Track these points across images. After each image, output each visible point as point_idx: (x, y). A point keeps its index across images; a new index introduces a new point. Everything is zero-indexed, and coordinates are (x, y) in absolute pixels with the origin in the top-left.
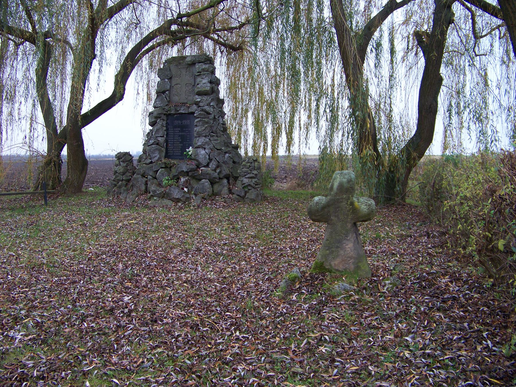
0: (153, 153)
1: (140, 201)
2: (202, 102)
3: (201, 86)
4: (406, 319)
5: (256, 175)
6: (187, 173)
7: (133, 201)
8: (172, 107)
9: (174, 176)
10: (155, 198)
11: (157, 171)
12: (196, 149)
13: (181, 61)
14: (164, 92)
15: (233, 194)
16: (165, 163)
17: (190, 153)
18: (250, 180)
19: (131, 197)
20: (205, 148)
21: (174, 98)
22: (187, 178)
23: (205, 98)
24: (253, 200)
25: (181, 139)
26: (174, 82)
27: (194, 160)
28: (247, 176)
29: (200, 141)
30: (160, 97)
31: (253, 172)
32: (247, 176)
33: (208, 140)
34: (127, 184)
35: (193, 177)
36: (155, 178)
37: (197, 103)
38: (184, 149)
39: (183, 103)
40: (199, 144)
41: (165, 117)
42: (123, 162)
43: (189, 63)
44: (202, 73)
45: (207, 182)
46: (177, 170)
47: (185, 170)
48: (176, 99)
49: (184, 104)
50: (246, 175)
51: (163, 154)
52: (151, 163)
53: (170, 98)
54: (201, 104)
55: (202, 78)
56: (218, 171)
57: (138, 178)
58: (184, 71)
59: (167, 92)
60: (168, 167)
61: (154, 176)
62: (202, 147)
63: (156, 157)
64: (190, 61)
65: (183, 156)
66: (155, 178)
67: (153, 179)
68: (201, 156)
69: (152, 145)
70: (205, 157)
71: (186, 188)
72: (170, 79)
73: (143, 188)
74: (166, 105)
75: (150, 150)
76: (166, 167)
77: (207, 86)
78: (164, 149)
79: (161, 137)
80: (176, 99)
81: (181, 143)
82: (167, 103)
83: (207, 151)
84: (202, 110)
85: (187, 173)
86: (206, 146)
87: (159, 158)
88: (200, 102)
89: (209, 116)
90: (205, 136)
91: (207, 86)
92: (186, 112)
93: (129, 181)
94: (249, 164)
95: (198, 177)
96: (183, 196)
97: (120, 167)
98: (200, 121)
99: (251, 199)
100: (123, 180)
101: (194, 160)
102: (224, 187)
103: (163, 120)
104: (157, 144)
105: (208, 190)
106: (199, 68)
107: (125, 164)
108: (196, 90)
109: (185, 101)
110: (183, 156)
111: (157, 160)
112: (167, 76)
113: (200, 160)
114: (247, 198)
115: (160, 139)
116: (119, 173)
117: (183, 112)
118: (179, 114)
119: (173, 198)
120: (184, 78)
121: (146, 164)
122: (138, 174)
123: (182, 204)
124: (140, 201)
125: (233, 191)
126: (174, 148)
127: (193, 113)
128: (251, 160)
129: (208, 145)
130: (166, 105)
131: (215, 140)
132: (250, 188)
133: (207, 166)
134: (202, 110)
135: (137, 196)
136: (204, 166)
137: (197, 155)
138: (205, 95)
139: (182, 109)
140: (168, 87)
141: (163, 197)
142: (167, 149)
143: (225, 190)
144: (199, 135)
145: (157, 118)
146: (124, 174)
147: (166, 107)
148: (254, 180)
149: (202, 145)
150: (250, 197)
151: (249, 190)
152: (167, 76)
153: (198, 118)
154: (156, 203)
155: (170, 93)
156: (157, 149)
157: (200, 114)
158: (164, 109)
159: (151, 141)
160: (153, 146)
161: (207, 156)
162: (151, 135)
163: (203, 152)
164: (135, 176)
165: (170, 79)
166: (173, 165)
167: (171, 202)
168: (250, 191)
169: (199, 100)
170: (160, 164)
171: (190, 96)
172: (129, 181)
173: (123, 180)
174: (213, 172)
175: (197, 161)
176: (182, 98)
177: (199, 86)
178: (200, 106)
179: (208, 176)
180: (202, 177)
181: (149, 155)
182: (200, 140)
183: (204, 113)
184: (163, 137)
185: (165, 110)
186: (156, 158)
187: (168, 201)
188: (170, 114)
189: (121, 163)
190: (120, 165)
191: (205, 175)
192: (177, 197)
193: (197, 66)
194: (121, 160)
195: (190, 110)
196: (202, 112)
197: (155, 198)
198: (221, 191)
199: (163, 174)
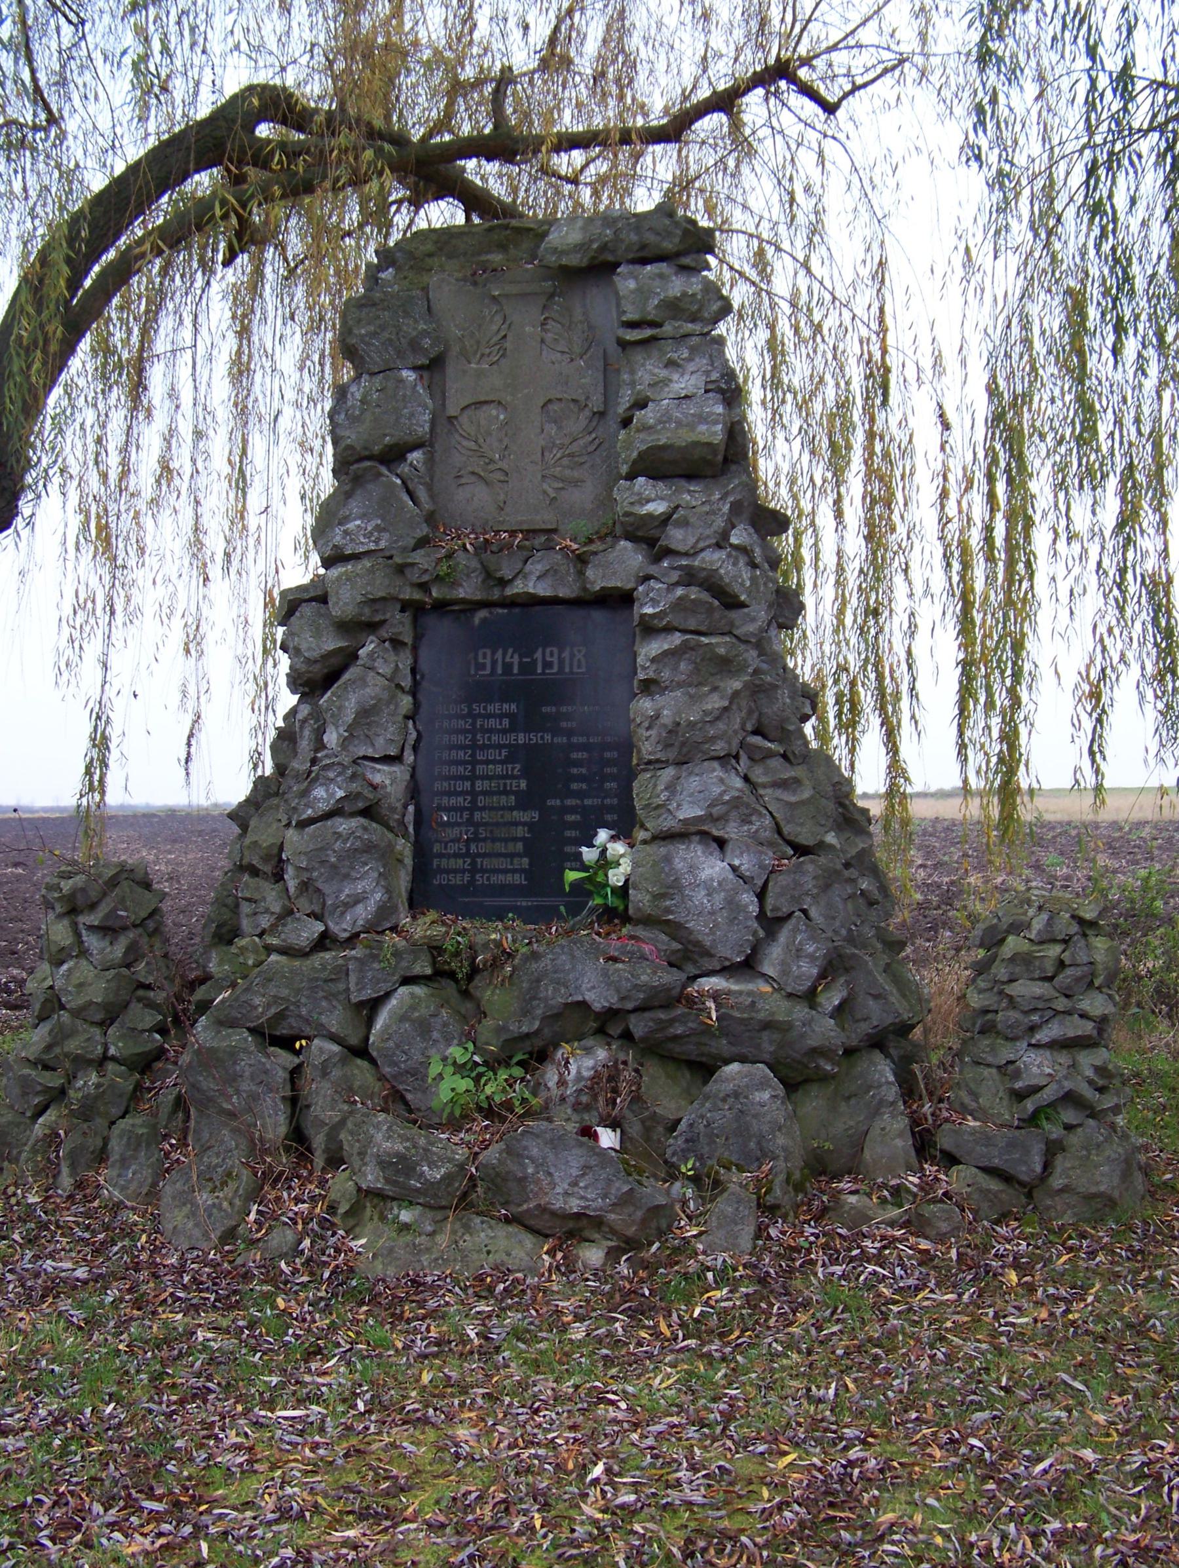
0: (339, 873)
1: (282, 1238)
2: (684, 523)
3: (665, 419)
4: (900, 1401)
5: (1102, 1022)
6: (607, 1024)
7: (230, 1235)
8: (461, 557)
9: (512, 1043)
10: (405, 1216)
11: (373, 1006)
12: (662, 850)
13: (496, 258)
14: (393, 456)
15: (951, 1160)
16: (435, 949)
17: (616, 877)
18: (1064, 1058)
19: (204, 1198)
20: (721, 843)
21: (461, 495)
22: (602, 1054)
23: (692, 495)
24: (1102, 1206)
25: (526, 773)
26: (460, 386)
27: (648, 921)
28: (1042, 1036)
29: (694, 793)
30: (375, 490)
31: (1085, 1005)
32: (1042, 1036)
33: (738, 783)
34: (138, 1087)
35: (656, 1049)
36: (361, 1051)
37: (648, 536)
38: (552, 846)
39: (530, 533)
40: (689, 811)
41: (400, 624)
42: (108, 930)
43: (574, 260)
44: (668, 329)
45: (763, 1085)
46: (531, 996)
47: (599, 998)
48: (473, 501)
49: (539, 537)
50: (1033, 1029)
51: (403, 880)
52: (324, 941)
53: (432, 496)
54: (677, 537)
55: (671, 364)
56: (832, 998)
57: (233, 1054)
58: (527, 321)
59: (415, 456)
60: (454, 975)
61: (354, 1041)
62: (704, 835)
63: (357, 900)
64: (579, 247)
65: (548, 890)
66: (361, 1051)
67: (343, 1061)
68: (700, 897)
69: (334, 813)
70: (732, 904)
71: (614, 1125)
72: (433, 367)
73: (274, 1124)
74: (422, 543)
75: (318, 855)
76: (440, 974)
77: (702, 418)
78: (404, 847)
79: (387, 759)
80: (473, 501)
81: (524, 801)
82: (424, 530)
83: (745, 862)
84: (690, 577)
85: (607, 1024)
86: (731, 831)
87: (385, 910)
88: (665, 520)
89: (734, 615)
90: (724, 760)
91: (702, 418)
92: (563, 592)
93: (146, 1064)
94: (1054, 950)
95: (690, 1050)
96: (627, 1199)
97: (85, 970)
98: (684, 648)
99: (1089, 1197)
100: (105, 1058)
101: (648, 921)
102: (876, 1113)
103: (397, 643)
104: (367, 812)
105: (781, 1140)
106: (643, 293)
107: (118, 951)
108: (631, 445)
109: (545, 519)
110: (548, 890)
111: (373, 927)
112: (415, 346)
113: (699, 927)
114: (1065, 1190)
115: (381, 775)
116: (77, 1013)
117: (543, 590)
118: (511, 603)
119: (543, 1209)
120: (525, 371)
121: (284, 951)
122: (226, 1023)
123: (613, 1255)
124: (282, 1238)
125: (945, 1141)
126: (476, 839)
127: (623, 599)
128: (1065, 925)
129: (746, 821)
130: (422, 543)
131: (783, 784)
132: (1069, 1115)
133: (748, 966)
134: (690, 577)
135: (255, 1194)
136: (728, 970)
137: (671, 888)
138: (690, 477)
139: (536, 567)
140: (422, 424)
141: (464, 1202)
142: (421, 852)
143: (891, 1135)
144: (685, 751)
145: (357, 627)
146: (110, 1015)
147: (418, 557)
148: (1088, 1060)
149: (711, 818)
150: (1084, 1185)
151: (1069, 1128)
152: (415, 346)
153: (669, 629)
154: (416, 1250)
155: (430, 461)
156: (369, 848)
157: (680, 605)
158: (401, 569)
159: (319, 792)
160: (343, 825)
161: (748, 899)
162: (305, 744)
163: (713, 868)
164: (203, 1031)
165: (433, 367)
166: (495, 964)
167: (529, 1240)
168: (1074, 1140)
169: (658, 508)
170: (397, 954)
171: (576, 483)
172: (146, 1064)
173: (105, 1058)
174: (800, 1012)
175: (674, 929)
176: (528, 502)
177: (647, 415)
178: (668, 552)
179: (768, 1044)
180: (723, 1046)
181: (304, 886)
182: (693, 783)
183: (705, 596)
184: (396, 759)
185: (414, 576)
186: (363, 913)
187: (502, 1231)
188: (441, 606)
189: (93, 942)
190: (84, 953)
191: (744, 1035)
192: (574, 1205)
193: (627, 282)
194: (94, 919)
195: (598, 579)
196: (694, 593)
197: (405, 1216)
198: (858, 1143)
199: (423, 1028)
